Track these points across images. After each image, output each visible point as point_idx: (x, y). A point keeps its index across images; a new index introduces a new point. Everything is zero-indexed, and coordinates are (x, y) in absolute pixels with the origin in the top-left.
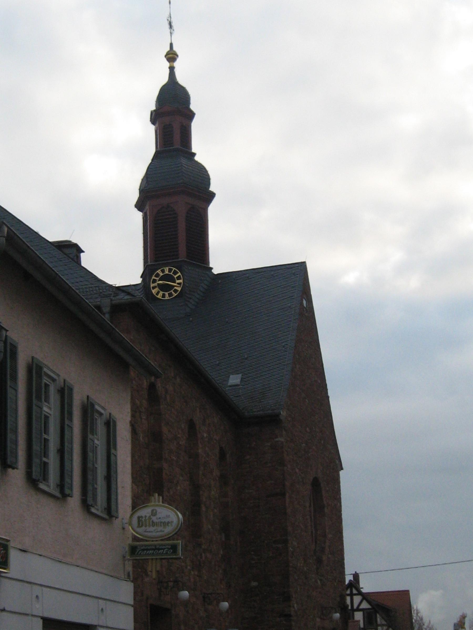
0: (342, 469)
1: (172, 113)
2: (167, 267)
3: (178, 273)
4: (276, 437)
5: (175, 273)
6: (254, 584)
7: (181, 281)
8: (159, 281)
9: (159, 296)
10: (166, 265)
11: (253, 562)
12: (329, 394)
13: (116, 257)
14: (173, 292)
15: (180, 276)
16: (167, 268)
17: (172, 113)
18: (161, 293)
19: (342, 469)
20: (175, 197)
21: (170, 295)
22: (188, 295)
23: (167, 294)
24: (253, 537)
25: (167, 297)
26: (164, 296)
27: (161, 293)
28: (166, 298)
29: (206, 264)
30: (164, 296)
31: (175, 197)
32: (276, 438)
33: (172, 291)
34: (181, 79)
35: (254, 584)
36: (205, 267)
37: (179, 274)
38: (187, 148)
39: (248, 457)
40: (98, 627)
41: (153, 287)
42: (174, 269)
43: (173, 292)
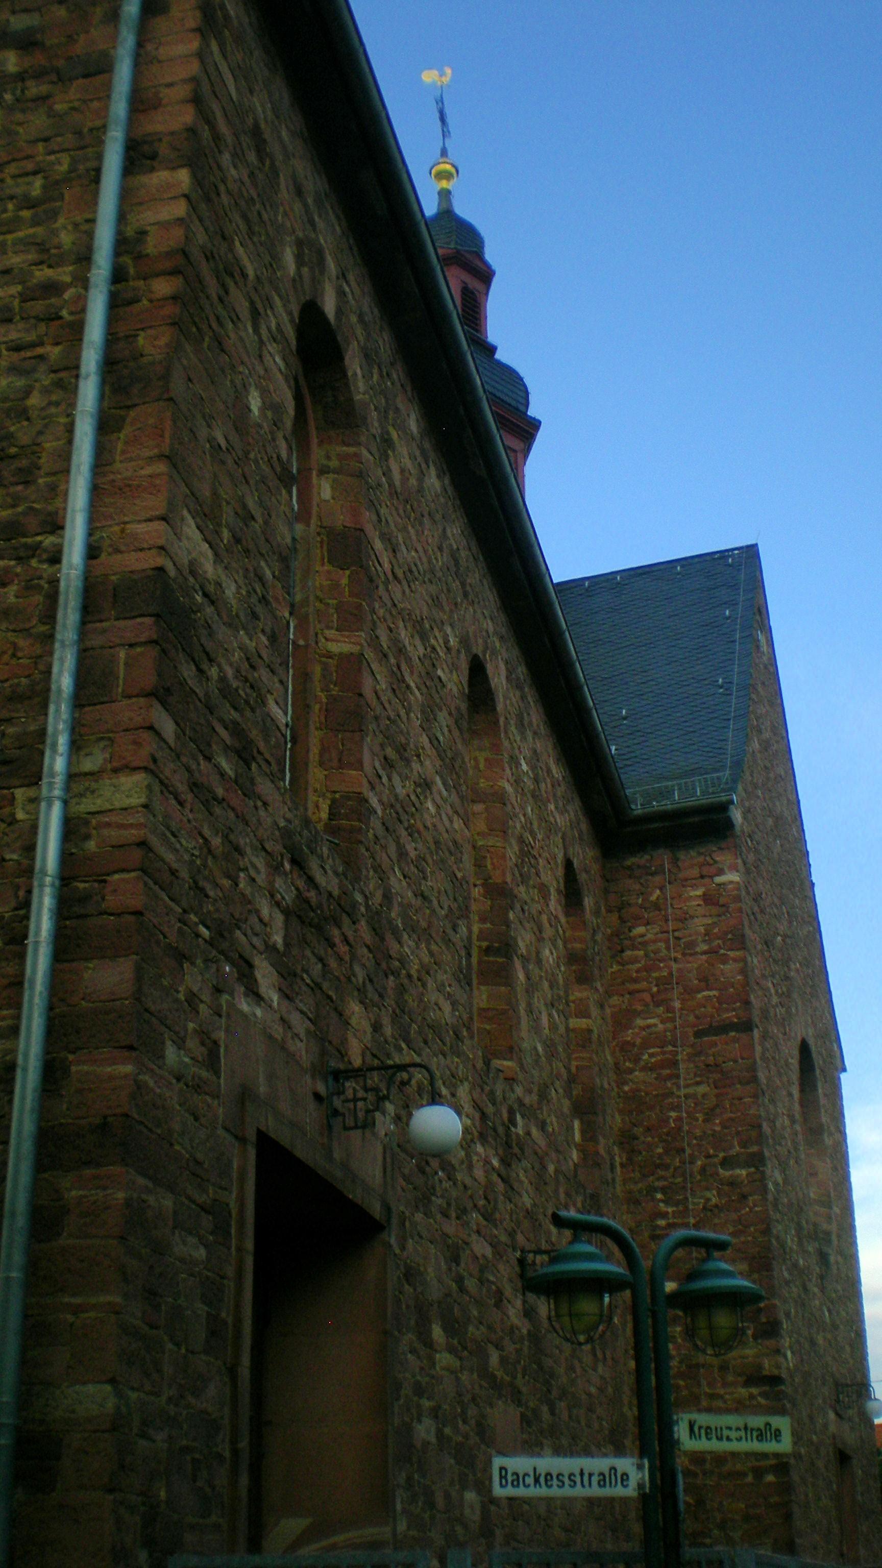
0: (844, 1070)
4: (721, 872)
11: (662, 1223)
19: (844, 1070)
24: (660, 1150)
32: (718, 875)
34: (462, 210)
38: (477, 331)
39: (641, 930)
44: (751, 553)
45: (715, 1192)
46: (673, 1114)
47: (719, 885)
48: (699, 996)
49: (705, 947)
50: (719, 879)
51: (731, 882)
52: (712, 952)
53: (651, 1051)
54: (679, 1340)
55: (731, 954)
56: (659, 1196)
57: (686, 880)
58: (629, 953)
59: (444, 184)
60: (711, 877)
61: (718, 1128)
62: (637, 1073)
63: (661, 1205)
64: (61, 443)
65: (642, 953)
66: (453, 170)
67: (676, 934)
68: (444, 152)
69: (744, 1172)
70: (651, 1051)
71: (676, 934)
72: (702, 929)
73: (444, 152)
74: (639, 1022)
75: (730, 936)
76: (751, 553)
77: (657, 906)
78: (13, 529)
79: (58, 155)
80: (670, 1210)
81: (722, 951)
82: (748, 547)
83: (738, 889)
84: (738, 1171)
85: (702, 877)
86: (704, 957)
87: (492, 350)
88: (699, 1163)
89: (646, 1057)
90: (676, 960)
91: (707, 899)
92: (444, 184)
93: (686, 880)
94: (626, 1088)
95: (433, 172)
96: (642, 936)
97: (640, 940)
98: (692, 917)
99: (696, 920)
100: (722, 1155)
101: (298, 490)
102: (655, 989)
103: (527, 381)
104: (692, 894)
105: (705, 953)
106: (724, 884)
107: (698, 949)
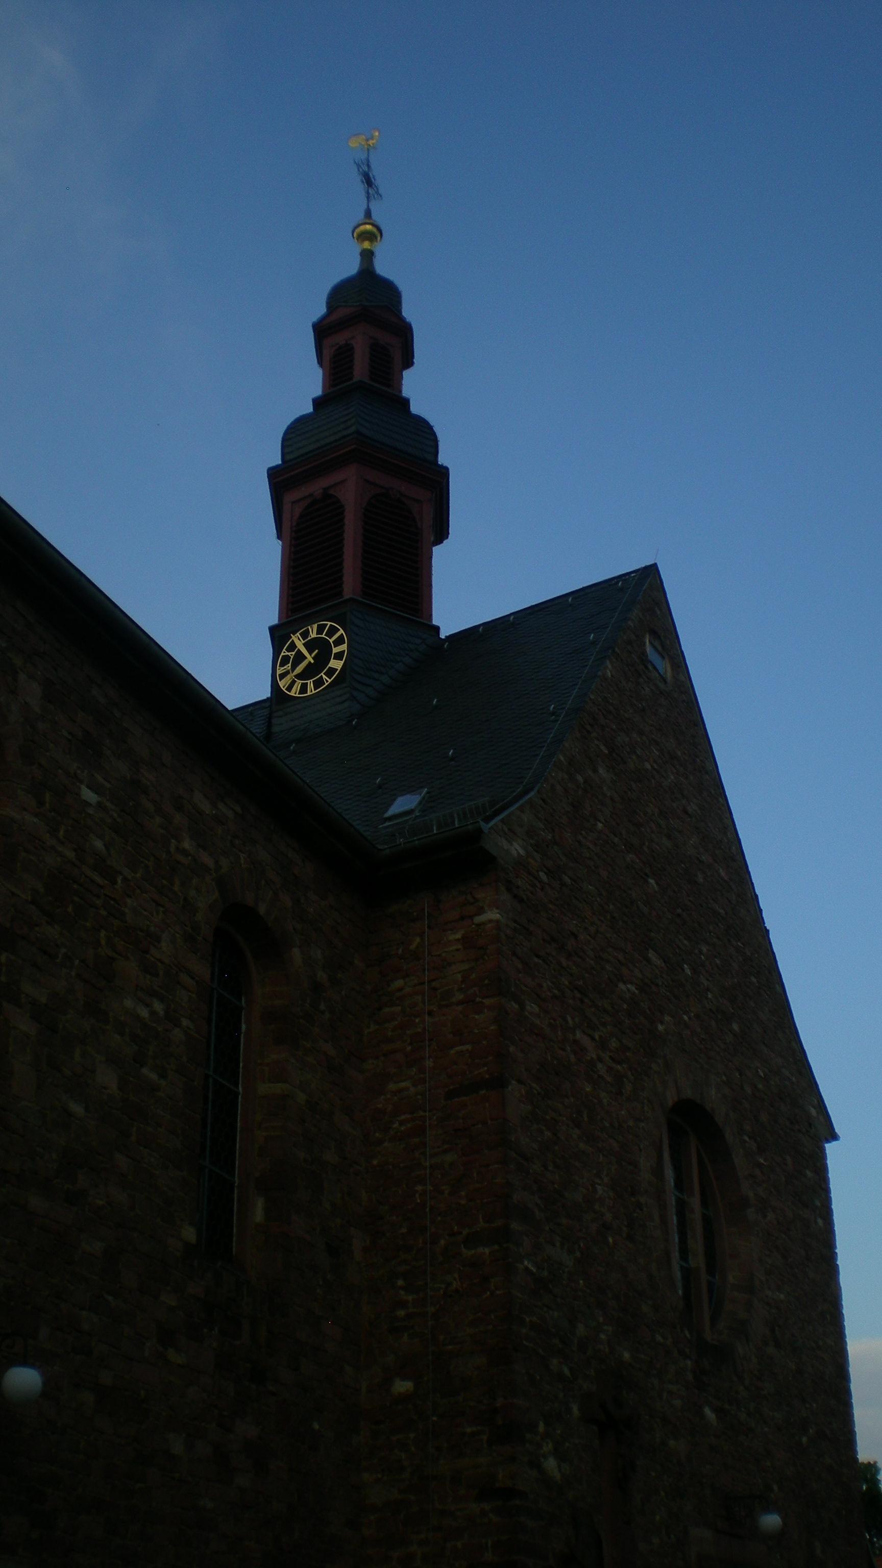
0: (834, 1137)
1: (365, 333)
4: (481, 911)
5: (333, 631)
6: (402, 1386)
7: (344, 647)
10: (310, 619)
11: (401, 1313)
12: (768, 925)
14: (324, 676)
16: (315, 626)
17: (365, 333)
19: (834, 1137)
20: (359, 490)
24: (404, 1230)
25: (311, 690)
26: (304, 689)
28: (309, 693)
30: (304, 689)
31: (359, 490)
32: (479, 914)
34: (382, 268)
35: (402, 1386)
37: (342, 631)
39: (399, 983)
42: (329, 623)
43: (324, 676)
44: (651, 573)
45: (456, 1275)
46: (419, 1188)
47: (479, 925)
48: (452, 1052)
49: (460, 996)
51: (490, 921)
53: (403, 1117)
54: (413, 1449)
55: (487, 1002)
56: (400, 1283)
58: (387, 1010)
59: (366, 245)
60: (471, 917)
61: (463, 1202)
62: (386, 1144)
63: (402, 1292)
65: (400, 1008)
66: (375, 230)
67: (434, 984)
68: (368, 214)
69: (487, 1251)
70: (403, 1117)
71: (434, 984)
73: (368, 214)
74: (392, 1086)
75: (486, 982)
76: (651, 573)
80: (410, 1298)
81: (478, 999)
82: (646, 568)
84: (481, 1250)
86: (460, 1008)
87: (406, 403)
88: (442, 1242)
89: (396, 1125)
90: (430, 1013)
92: (366, 245)
94: (375, 1162)
95: (355, 235)
96: (400, 989)
100: (465, 1232)
102: (409, 1048)
103: (436, 429)
104: (451, 937)
105: (460, 1003)
106: (483, 924)
107: (454, 1000)
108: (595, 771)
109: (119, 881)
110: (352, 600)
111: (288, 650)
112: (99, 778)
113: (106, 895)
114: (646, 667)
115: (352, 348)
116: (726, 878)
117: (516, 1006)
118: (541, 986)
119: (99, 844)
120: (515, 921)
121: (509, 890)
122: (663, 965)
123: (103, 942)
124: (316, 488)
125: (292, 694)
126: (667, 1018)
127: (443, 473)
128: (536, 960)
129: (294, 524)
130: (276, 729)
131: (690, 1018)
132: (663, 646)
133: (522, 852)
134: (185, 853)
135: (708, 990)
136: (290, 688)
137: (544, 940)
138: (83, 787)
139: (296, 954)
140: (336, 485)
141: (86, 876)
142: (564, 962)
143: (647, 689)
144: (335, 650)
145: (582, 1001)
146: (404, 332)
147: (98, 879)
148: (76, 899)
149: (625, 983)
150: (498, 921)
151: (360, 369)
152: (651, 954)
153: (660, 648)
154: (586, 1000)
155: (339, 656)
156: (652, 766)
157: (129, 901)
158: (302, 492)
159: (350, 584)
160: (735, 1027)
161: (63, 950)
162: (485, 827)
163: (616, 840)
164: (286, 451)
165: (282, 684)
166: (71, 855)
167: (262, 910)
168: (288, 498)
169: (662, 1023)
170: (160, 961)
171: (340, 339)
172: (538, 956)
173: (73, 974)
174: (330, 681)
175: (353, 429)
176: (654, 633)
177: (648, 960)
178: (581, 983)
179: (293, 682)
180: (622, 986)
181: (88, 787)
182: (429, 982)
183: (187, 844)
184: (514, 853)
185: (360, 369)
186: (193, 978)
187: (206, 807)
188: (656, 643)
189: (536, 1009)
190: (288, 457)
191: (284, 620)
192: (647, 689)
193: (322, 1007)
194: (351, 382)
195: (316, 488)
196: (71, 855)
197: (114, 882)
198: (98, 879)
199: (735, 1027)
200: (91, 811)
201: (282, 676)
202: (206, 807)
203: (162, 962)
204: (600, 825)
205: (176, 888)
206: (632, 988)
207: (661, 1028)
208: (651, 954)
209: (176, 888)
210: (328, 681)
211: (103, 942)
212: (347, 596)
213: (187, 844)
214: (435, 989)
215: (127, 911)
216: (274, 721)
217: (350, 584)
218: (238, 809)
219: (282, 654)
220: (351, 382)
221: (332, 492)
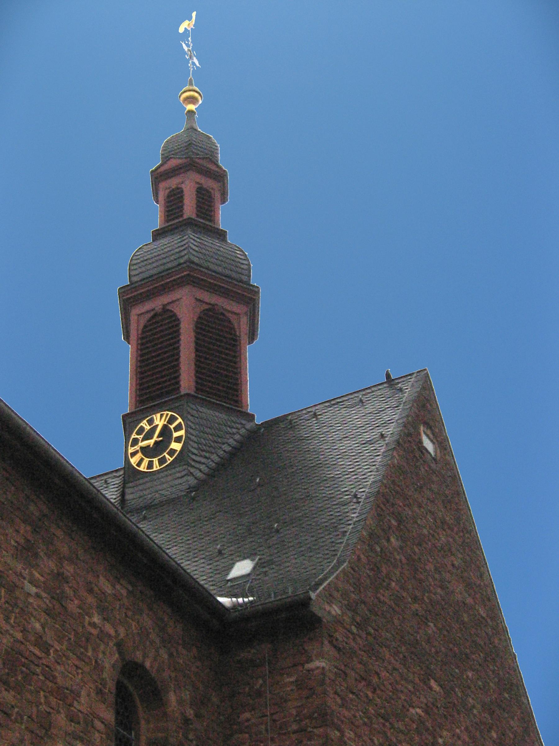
2: (158, 413)
3: (177, 419)
7: (182, 433)
8: (142, 441)
9: (143, 468)
13: (98, 431)
15: (180, 423)
18: (146, 461)
20: (189, 330)
21: (162, 461)
22: (194, 457)
23: (156, 461)
25: (156, 466)
26: (150, 465)
27: (146, 461)
28: (155, 469)
29: (242, 407)
30: (150, 465)
33: (165, 454)
36: (239, 411)
37: (180, 420)
38: (210, 221)
39: (247, 715)
40: (328, 415)
41: (131, 454)
49: (295, 727)
50: (308, 666)
51: (318, 668)
52: (302, 730)
57: (282, 669)
60: (303, 665)
64: (41, 578)
67: (274, 717)
71: (274, 717)
72: (294, 712)
77: (259, 694)
78: (13, 658)
79: (348, 627)
81: (310, 729)
83: (323, 674)
85: (295, 665)
91: (300, 685)
93: (282, 669)
96: (248, 720)
97: (246, 724)
98: (286, 701)
99: (289, 703)
101: (221, 596)
106: (312, 670)
108: (388, 540)
109: (51, 651)
110: (188, 395)
111: (138, 433)
112: (37, 575)
113: (43, 664)
114: (422, 452)
115: (182, 191)
116: (484, 615)
117: (339, 734)
118: (355, 716)
119: (38, 626)
120: (336, 667)
121: (331, 642)
122: (441, 691)
123: (42, 700)
124: (157, 304)
125: (141, 469)
126: (445, 733)
127: (255, 291)
128: (351, 696)
129: (140, 332)
130: (128, 497)
131: (461, 731)
132: (433, 434)
133: (339, 612)
134: (94, 625)
135: (474, 707)
136: (139, 464)
137: (356, 680)
138: (26, 582)
139: (172, 698)
140: (173, 302)
141: (30, 651)
142: (370, 694)
143: (422, 469)
144: (175, 435)
145: (384, 725)
146: (220, 177)
147: (37, 652)
148: (24, 669)
149: (413, 707)
150: (323, 668)
151: (189, 208)
152: (433, 683)
153: (431, 436)
154: (387, 724)
155: (178, 440)
156: (428, 531)
157: (58, 667)
158: (148, 306)
159: (187, 381)
160: (494, 735)
161: (16, 710)
162: (313, 595)
163: (405, 594)
164: (133, 273)
165: (133, 461)
166: (19, 636)
167: (147, 664)
168: (135, 312)
169: (441, 737)
170: (79, 711)
171: (173, 182)
172: (353, 693)
173: (23, 727)
174: (171, 459)
175: (186, 257)
176: (426, 424)
177: (431, 688)
178: (383, 711)
179: (142, 460)
180: (412, 711)
181: (29, 582)
182: (272, 714)
183: (96, 619)
184: (333, 613)
185: (189, 208)
186: (103, 722)
187: (108, 589)
188: (429, 432)
189: (352, 735)
190: (135, 279)
191: (134, 410)
192: (422, 469)
193: (191, 736)
194: (181, 219)
195: (157, 304)
196: (19, 636)
197: (47, 653)
198: (37, 652)
199: (494, 735)
200: (31, 600)
201: (133, 454)
202: (108, 589)
203: (81, 712)
204: (393, 584)
205: (90, 654)
206: (419, 711)
207: (440, 741)
208: (433, 683)
209: (90, 654)
210: (170, 459)
211: (42, 700)
212: (183, 391)
213: (96, 619)
214: (274, 721)
215: (57, 675)
216: (128, 491)
217: (187, 381)
218: (131, 588)
219: (133, 437)
220: (181, 219)
221: (169, 307)
